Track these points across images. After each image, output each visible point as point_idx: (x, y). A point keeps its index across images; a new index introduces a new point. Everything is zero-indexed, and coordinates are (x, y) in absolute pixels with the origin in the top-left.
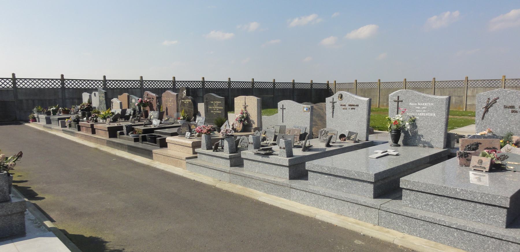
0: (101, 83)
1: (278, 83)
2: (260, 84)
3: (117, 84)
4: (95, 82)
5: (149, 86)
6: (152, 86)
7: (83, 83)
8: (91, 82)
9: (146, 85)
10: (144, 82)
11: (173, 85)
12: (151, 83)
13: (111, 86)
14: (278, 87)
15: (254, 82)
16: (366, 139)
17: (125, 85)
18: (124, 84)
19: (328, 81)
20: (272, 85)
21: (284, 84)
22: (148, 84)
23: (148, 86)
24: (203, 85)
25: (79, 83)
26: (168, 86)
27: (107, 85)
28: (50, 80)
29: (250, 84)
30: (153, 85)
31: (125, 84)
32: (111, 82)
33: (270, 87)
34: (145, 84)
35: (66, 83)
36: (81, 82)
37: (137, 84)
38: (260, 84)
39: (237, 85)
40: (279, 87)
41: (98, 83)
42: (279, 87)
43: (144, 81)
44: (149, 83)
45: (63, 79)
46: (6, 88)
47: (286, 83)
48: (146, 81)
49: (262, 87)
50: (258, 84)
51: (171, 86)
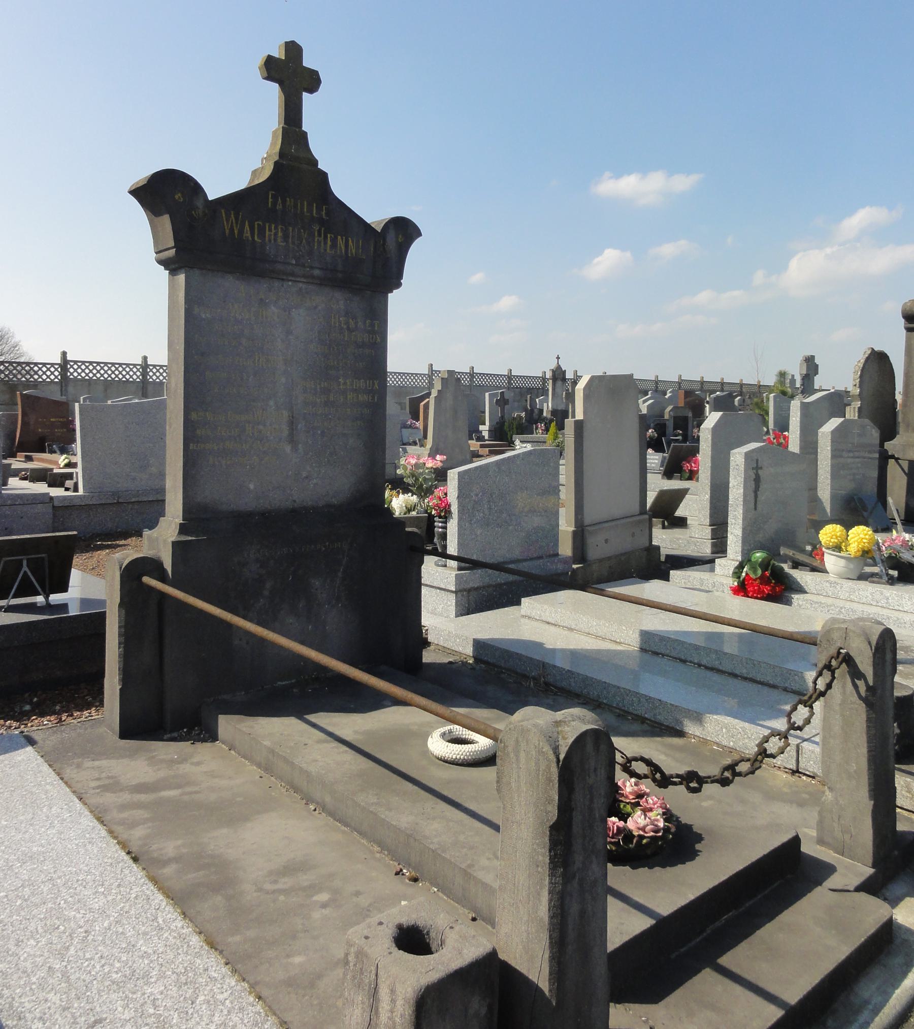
0: (56, 369)
1: (395, 373)
2: (395, 377)
3: (91, 371)
4: (42, 367)
5: (113, 376)
6: (120, 376)
7: (42, 371)
8: (104, 366)
9: (154, 374)
10: (151, 367)
11: (142, 374)
12: (117, 369)
13: (77, 374)
14: (393, 382)
15: (474, 373)
16: (710, 521)
17: (122, 375)
18: (113, 372)
19: (473, 368)
20: (426, 381)
21: (404, 377)
22: (160, 372)
23: (109, 376)
24: (144, 374)
25: (40, 371)
26: (133, 371)
27: (70, 372)
28: (14, 365)
29: (424, 378)
30: (156, 376)
31: (85, 369)
32: (46, 367)
33: (422, 383)
34: (136, 375)
35: (70, 368)
36: (44, 369)
37: (52, 373)
38: (408, 377)
39: (399, 380)
40: (416, 383)
41: (79, 367)
42: (395, 382)
43: (151, 365)
44: (113, 369)
45: (65, 364)
46: (31, 381)
47: (480, 375)
48: (154, 366)
49: (395, 382)
50: (395, 377)
51: (137, 376)
